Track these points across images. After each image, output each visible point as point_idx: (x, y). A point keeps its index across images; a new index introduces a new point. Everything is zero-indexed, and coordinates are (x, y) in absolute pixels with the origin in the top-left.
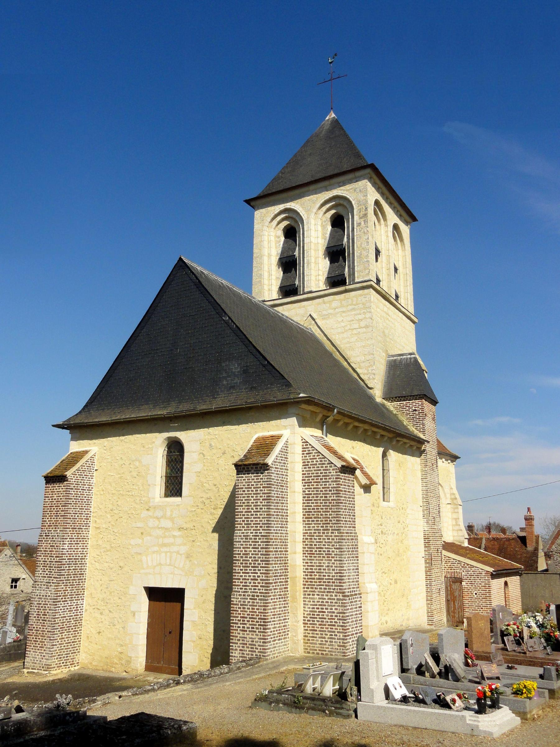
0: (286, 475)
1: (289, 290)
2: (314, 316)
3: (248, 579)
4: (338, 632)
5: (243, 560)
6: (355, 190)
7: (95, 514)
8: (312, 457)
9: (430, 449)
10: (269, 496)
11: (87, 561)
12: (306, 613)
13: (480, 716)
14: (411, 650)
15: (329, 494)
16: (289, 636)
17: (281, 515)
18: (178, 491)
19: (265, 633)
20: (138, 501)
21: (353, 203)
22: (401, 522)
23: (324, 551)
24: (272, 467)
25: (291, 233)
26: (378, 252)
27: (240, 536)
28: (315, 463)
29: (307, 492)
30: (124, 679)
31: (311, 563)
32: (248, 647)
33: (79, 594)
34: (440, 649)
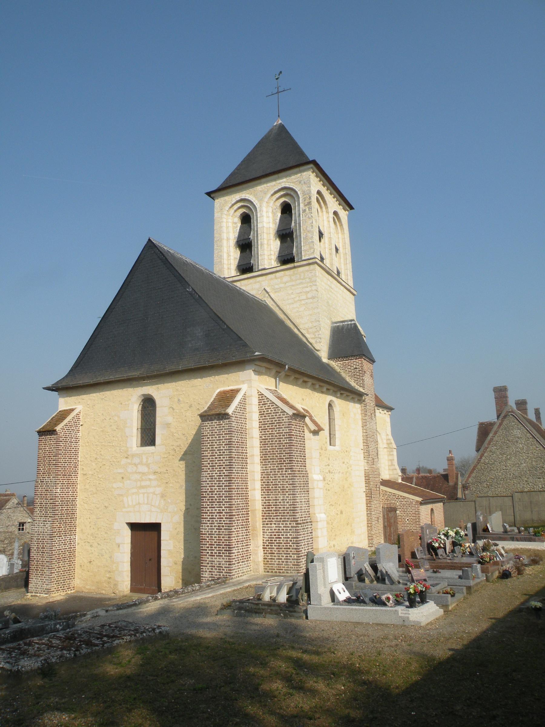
0: (245, 424)
1: (246, 268)
2: (268, 290)
3: (214, 513)
4: (292, 554)
5: (209, 497)
6: (300, 183)
7: (82, 463)
8: (267, 407)
9: (370, 400)
10: (230, 442)
11: (77, 503)
12: (265, 539)
13: (410, 609)
14: (353, 562)
15: (282, 438)
16: (251, 559)
17: (242, 458)
18: (152, 441)
19: (230, 556)
20: (118, 451)
21: (299, 193)
22: (346, 463)
23: (279, 487)
24: (232, 417)
25: (246, 219)
26: (321, 235)
27: (207, 476)
28: (270, 412)
29: (263, 438)
30: (113, 599)
31: (269, 497)
32: (216, 569)
33: (72, 529)
34: (377, 560)
